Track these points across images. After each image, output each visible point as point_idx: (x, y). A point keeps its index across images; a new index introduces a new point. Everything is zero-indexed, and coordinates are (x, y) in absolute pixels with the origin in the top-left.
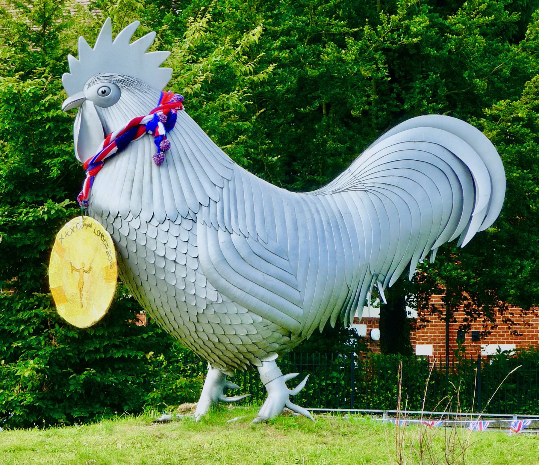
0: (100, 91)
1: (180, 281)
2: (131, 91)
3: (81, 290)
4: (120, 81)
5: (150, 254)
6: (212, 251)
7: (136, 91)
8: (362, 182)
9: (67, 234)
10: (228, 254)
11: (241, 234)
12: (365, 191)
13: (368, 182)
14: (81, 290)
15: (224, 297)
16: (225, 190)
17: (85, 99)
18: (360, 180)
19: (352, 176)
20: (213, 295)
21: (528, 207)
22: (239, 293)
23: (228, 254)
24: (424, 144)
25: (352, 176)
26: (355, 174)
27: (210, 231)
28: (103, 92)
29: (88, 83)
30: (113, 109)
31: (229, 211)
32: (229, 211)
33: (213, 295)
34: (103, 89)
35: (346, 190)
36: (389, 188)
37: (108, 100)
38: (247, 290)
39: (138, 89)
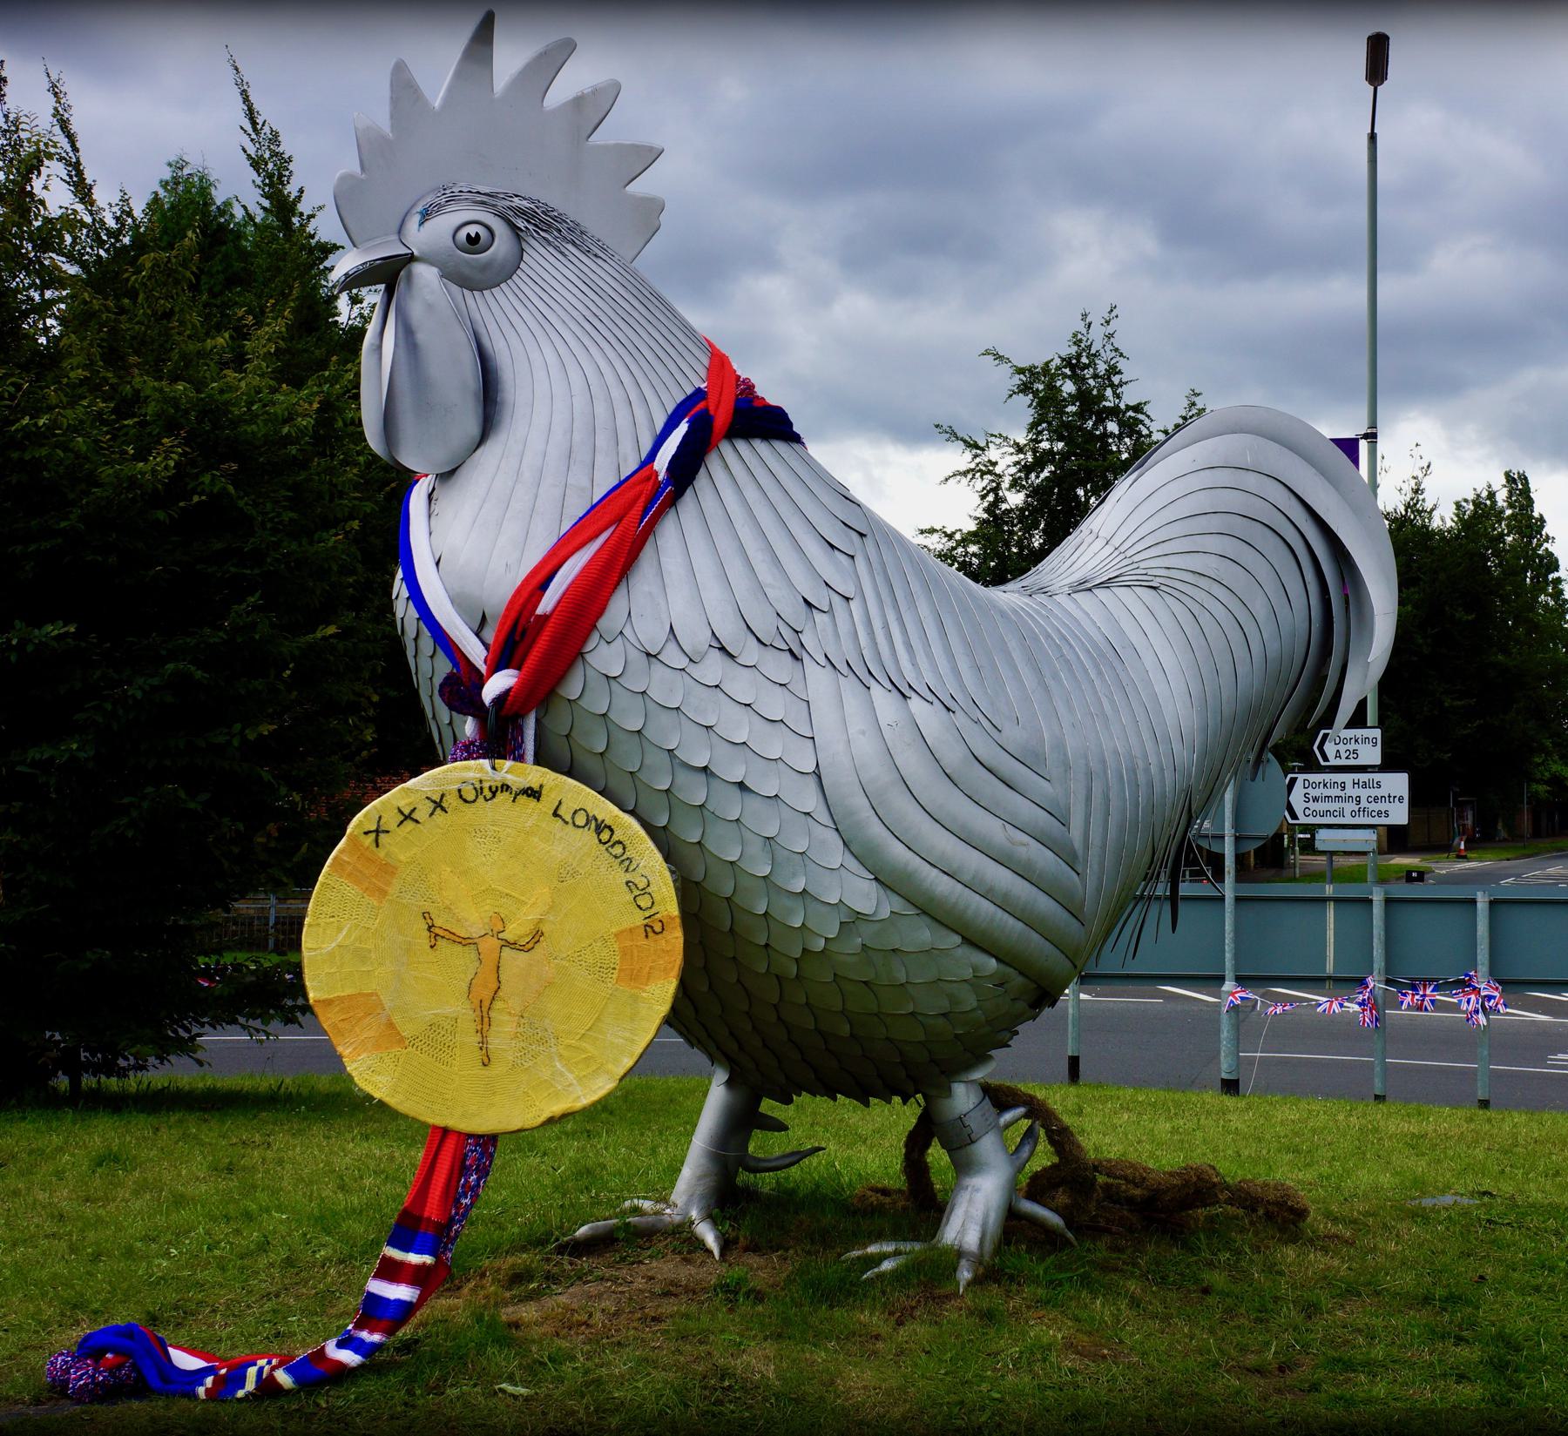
0: (462, 234)
1: (755, 847)
2: (555, 248)
3: (484, 1020)
4: (520, 212)
5: (657, 760)
6: (866, 747)
7: (570, 247)
8: (1142, 565)
9: (408, 817)
10: (913, 764)
11: (936, 701)
12: (1154, 588)
13: (1154, 565)
14: (484, 1020)
15: (896, 899)
16: (859, 560)
17: (411, 258)
18: (1136, 558)
19: (1109, 549)
20: (863, 895)
21: (369, 698)
22: (943, 886)
23: (913, 764)
24: (1252, 477)
25: (1109, 549)
26: (1116, 542)
27: (849, 685)
28: (473, 240)
29: (419, 208)
30: (502, 296)
31: (886, 626)
32: (886, 626)
33: (863, 895)
34: (472, 230)
35: (1105, 585)
36: (1202, 582)
37: (486, 267)
38: (966, 878)
39: (574, 244)
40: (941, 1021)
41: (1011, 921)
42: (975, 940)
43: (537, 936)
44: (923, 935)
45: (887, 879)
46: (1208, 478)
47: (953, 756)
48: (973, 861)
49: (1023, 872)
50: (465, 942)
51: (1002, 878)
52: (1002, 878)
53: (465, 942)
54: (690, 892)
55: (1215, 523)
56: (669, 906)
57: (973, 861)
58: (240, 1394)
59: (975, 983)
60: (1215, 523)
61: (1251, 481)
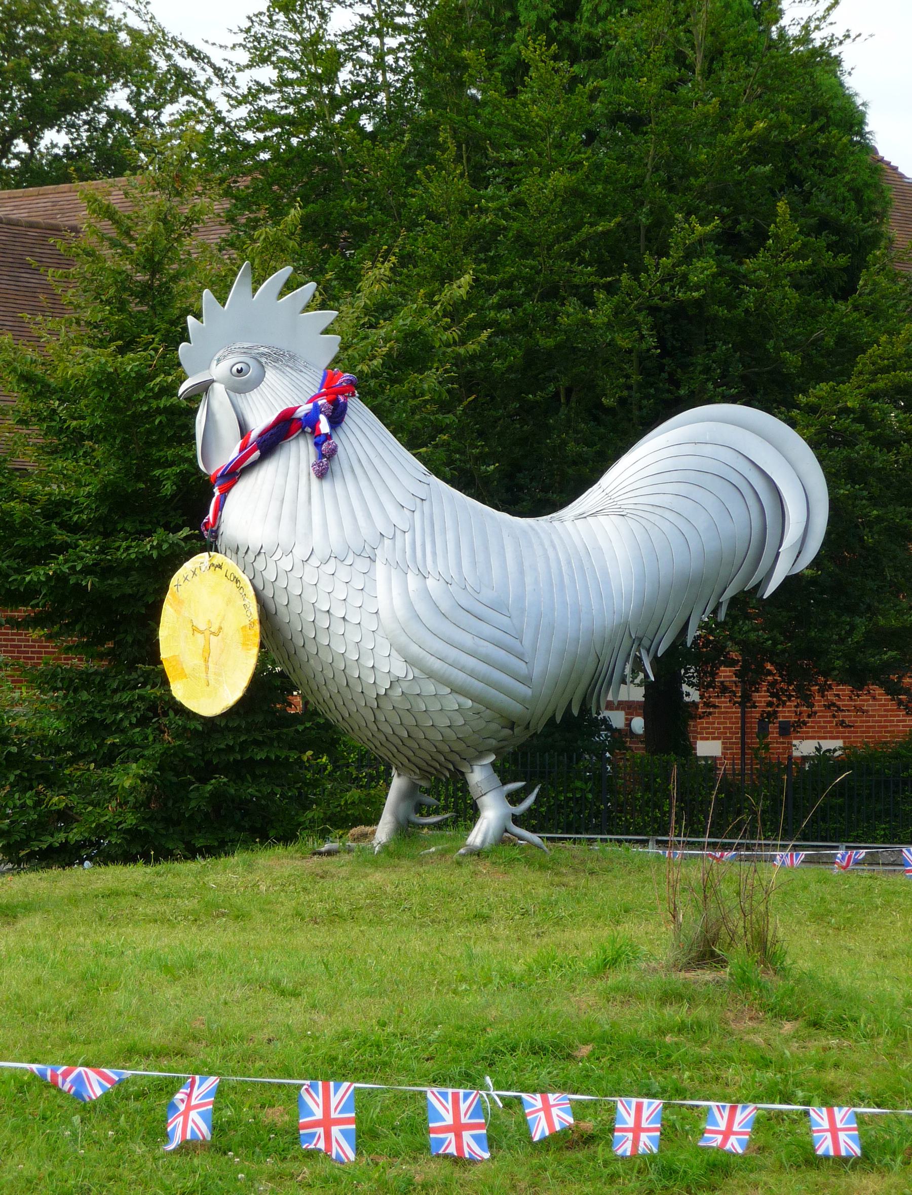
6: (398, 602)
10: (422, 608)
15: (416, 670)
22: (437, 665)
23: (422, 608)
28: (239, 371)
30: (254, 395)
33: (453, 702)
34: (239, 366)
37: (246, 382)
40: (448, 730)
41: (476, 682)
42: (456, 690)
43: (221, 628)
44: (430, 688)
45: (410, 661)
46: (674, 451)
47: (445, 606)
48: (453, 653)
49: (502, 668)
50: (202, 632)
51: (471, 662)
52: (471, 662)
53: (202, 632)
54: (268, 618)
55: (675, 476)
56: (256, 616)
57: (453, 653)
58: (171, 1147)
59: (460, 710)
60: (675, 476)
61: (708, 450)
